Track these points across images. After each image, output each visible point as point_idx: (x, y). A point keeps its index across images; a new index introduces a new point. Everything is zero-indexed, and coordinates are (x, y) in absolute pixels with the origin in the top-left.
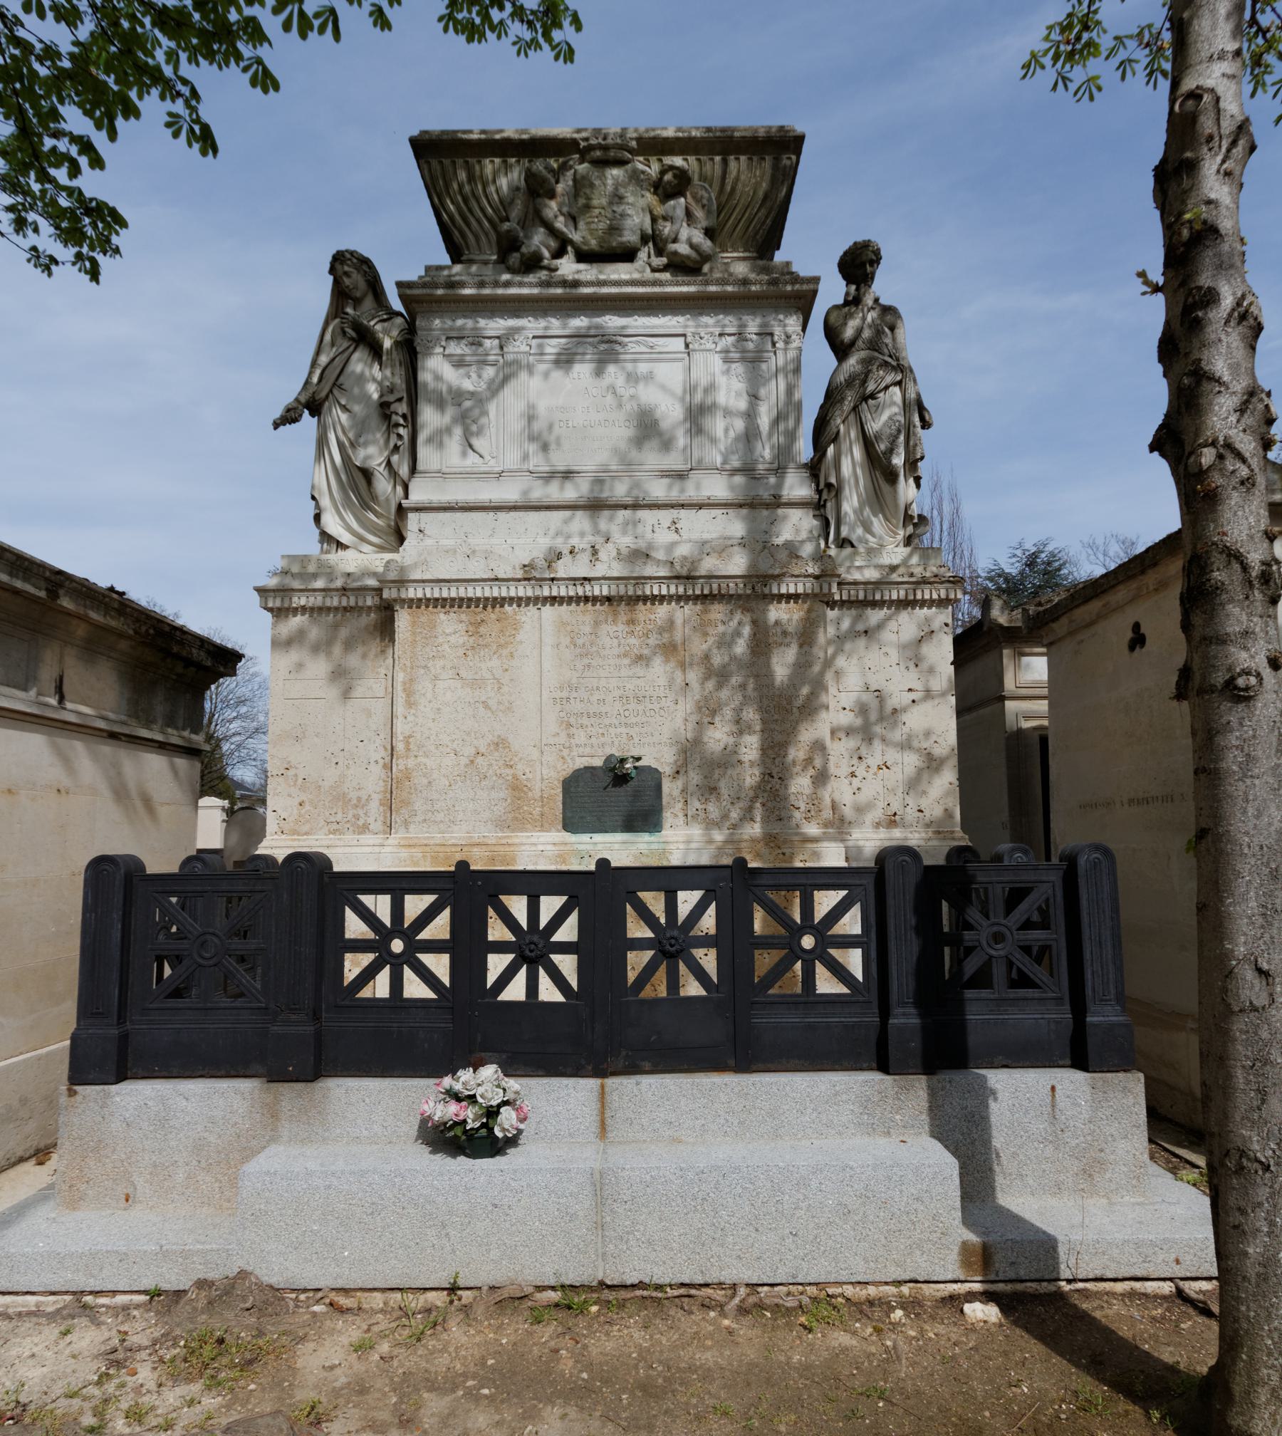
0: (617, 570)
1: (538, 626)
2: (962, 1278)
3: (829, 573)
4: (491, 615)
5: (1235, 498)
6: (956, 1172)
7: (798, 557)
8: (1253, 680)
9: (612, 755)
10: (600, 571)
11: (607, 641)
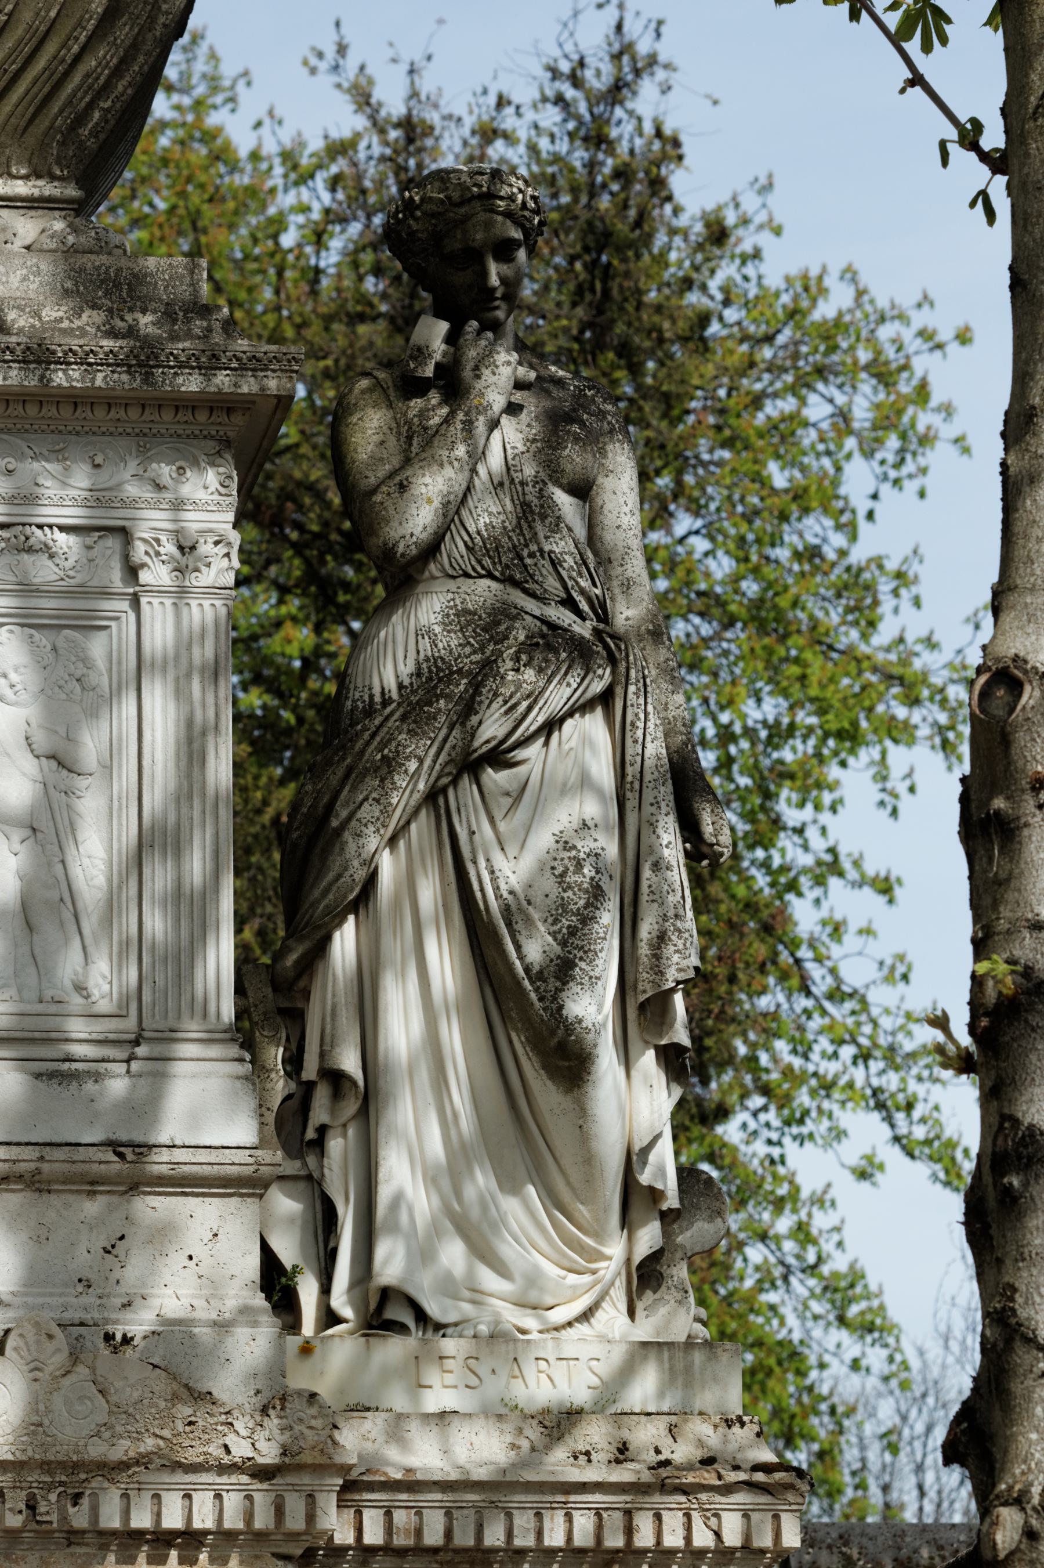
3: (307, 1458)
7: (204, 1398)
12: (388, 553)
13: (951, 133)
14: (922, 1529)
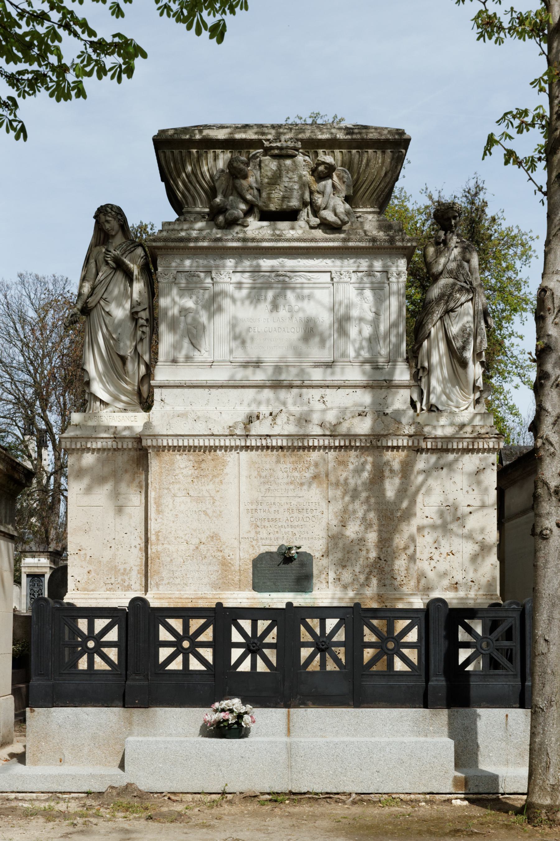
0: (291, 429)
1: (237, 464)
2: (454, 792)
4: (208, 456)
5: (548, 460)
6: (453, 746)
8: (548, 532)
9: (283, 545)
10: (276, 430)
11: (280, 474)
12: (433, 274)
13: (537, 189)
14: (524, 447)
